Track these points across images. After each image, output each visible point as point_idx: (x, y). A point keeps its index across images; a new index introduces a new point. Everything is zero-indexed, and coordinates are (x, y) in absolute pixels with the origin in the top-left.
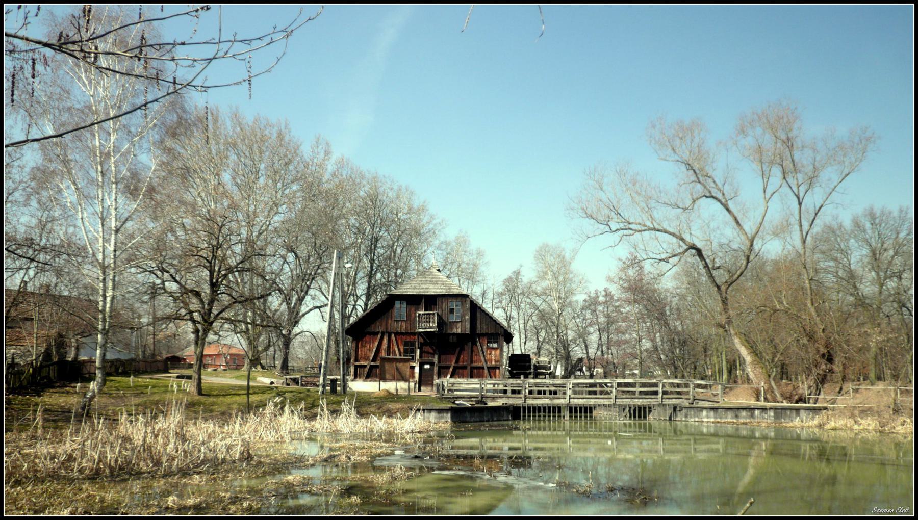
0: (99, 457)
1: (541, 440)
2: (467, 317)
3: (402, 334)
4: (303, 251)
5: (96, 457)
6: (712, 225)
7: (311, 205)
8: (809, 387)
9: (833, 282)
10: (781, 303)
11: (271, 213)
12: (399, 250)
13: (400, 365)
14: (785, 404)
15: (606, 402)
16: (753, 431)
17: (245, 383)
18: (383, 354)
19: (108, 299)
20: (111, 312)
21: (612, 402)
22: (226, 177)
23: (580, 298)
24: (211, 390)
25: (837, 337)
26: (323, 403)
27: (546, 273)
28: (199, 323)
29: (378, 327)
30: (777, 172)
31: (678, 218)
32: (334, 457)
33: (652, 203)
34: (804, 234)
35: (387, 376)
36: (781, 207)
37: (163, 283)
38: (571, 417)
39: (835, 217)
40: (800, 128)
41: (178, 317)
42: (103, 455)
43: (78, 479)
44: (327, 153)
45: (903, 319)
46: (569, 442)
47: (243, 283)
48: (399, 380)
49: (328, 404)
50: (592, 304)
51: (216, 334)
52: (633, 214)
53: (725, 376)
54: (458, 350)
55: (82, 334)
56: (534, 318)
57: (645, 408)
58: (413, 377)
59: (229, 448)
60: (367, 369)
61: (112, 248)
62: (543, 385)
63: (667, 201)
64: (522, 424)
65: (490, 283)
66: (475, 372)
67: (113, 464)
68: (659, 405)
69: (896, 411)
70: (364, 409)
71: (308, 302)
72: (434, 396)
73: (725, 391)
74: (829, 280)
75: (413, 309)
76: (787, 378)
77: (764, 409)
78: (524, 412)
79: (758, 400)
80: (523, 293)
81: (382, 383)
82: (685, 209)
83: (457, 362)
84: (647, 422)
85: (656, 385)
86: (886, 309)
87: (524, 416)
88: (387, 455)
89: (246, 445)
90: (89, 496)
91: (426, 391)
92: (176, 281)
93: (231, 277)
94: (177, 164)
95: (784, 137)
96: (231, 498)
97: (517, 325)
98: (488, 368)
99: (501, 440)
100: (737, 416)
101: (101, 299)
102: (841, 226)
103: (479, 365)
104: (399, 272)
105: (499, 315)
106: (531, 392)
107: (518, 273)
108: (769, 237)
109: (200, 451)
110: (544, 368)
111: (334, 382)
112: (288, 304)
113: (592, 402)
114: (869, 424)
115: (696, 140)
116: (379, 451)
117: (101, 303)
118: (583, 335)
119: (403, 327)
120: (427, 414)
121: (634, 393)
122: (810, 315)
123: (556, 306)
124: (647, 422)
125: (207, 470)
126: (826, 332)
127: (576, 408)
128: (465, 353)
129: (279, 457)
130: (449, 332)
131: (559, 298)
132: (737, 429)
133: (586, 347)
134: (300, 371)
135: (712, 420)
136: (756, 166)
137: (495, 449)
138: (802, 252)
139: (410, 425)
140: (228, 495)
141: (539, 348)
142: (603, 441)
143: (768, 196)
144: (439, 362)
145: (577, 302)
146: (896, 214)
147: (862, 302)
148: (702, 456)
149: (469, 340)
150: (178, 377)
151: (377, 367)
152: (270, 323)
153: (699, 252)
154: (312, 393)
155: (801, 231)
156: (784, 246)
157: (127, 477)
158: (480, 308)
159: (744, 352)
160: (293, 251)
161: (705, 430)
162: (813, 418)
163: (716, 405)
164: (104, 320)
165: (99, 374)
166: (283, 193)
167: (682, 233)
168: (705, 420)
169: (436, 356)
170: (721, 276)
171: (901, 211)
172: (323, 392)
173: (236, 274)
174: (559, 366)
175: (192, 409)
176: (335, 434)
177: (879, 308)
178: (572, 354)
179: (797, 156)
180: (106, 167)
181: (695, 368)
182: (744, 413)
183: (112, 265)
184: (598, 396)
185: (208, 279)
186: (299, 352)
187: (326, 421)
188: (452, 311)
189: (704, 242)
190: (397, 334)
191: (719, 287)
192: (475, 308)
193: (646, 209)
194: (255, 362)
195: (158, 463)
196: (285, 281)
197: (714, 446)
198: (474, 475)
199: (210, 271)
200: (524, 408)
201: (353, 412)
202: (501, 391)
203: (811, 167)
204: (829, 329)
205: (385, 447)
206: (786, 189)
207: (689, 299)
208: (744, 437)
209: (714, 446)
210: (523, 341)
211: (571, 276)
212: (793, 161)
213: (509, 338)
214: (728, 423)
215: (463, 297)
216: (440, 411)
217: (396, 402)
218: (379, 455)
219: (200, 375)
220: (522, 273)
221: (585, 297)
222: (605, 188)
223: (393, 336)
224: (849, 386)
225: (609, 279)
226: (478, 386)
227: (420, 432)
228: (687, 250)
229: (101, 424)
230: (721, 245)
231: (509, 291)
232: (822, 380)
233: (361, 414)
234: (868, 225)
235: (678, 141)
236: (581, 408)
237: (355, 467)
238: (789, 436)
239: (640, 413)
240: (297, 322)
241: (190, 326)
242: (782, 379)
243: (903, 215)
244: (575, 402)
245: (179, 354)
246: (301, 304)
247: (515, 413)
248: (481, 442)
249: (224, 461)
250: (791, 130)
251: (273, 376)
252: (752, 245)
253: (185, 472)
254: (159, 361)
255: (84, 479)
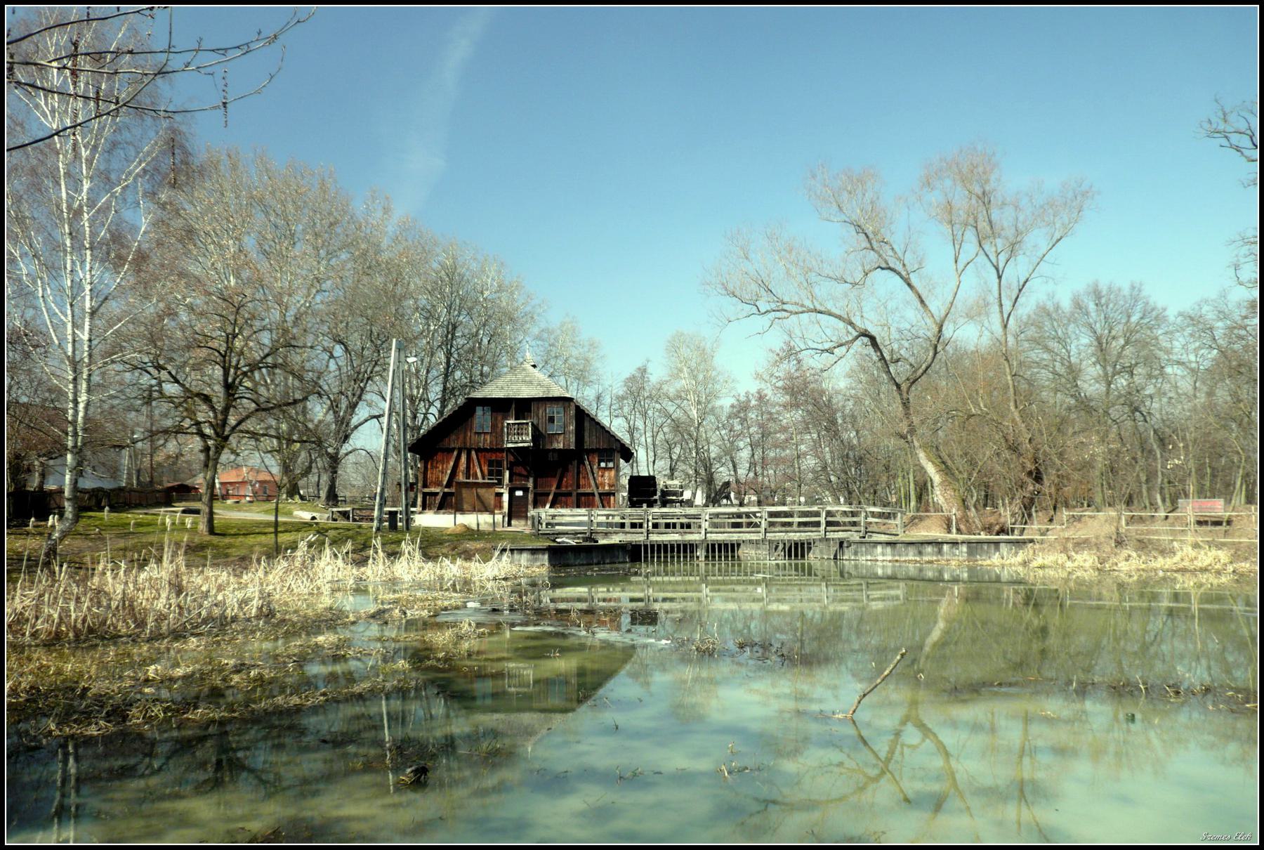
0: (60, 618)
1: (682, 587)
2: (572, 428)
3: (485, 450)
4: (355, 341)
5: (56, 616)
6: (891, 305)
7: (365, 279)
8: (1013, 515)
9: (1048, 380)
10: (976, 404)
11: (301, 288)
12: (485, 341)
13: (482, 491)
14: (983, 536)
15: (754, 537)
16: (941, 572)
17: (273, 519)
18: (461, 478)
19: (81, 406)
20: (85, 423)
21: (760, 536)
22: (250, 242)
23: (725, 403)
24: (228, 526)
25: (1047, 449)
26: (377, 542)
27: (681, 371)
28: (209, 437)
29: (454, 441)
30: (970, 235)
31: (846, 295)
32: (384, 611)
33: (813, 277)
34: (1005, 316)
35: (465, 507)
36: (976, 282)
37: (160, 384)
38: (707, 557)
39: (1051, 296)
40: (999, 180)
41: (179, 430)
42: (65, 611)
43: (30, 646)
44: (386, 210)
45: (1136, 427)
46: (705, 590)
47: (270, 386)
48: (480, 511)
49: (383, 544)
50: (741, 409)
51: (233, 452)
52: (789, 291)
53: (913, 503)
54: (559, 471)
55: (49, 455)
56: (666, 429)
57: (803, 544)
58: (501, 507)
59: (244, 602)
60: (439, 498)
61: (86, 337)
62: (673, 516)
63: (831, 274)
64: (645, 568)
65: (607, 384)
66: (583, 500)
67: (79, 626)
68: (820, 540)
69: (1119, 543)
70: (433, 550)
71: (362, 412)
72: (527, 532)
73: (913, 522)
74: (1044, 376)
75: (500, 418)
76: (993, 506)
77: (955, 544)
78: (646, 552)
79: (949, 532)
80: (650, 397)
81: (458, 516)
82: (854, 284)
83: (559, 487)
84: (806, 562)
85: (817, 514)
86: (1114, 413)
87: (646, 557)
88: (457, 608)
89: (266, 597)
90: (42, 666)
91: (519, 526)
92: (177, 381)
93: (257, 375)
94: (178, 223)
95: (978, 191)
96: (235, 666)
97: (643, 439)
98: (600, 494)
99: (618, 589)
100: (920, 553)
101: (71, 405)
102: (1057, 308)
103: (589, 491)
104: (486, 369)
105: (618, 427)
106: (655, 526)
107: (643, 371)
108: (961, 321)
109: (201, 606)
110: (675, 494)
111: (393, 515)
112: (335, 412)
113: (735, 537)
114: (1085, 562)
115: (869, 195)
116: (446, 603)
117: (71, 412)
118: (730, 452)
119: (485, 441)
120: (516, 556)
121: (790, 524)
122: (1013, 420)
123: (694, 413)
124: (806, 562)
125: (209, 633)
126: (1034, 443)
127: (713, 546)
128: (569, 475)
129: (310, 612)
130: (548, 447)
131: (699, 403)
132: (921, 570)
133: (734, 466)
134: (353, 502)
135: (889, 558)
136: (946, 229)
137: (610, 600)
138: (1003, 340)
139: (491, 572)
140: (232, 662)
141: (672, 470)
142: (751, 588)
143: (961, 267)
144: (535, 486)
145: (722, 407)
146: (1126, 292)
147: (1085, 405)
148: (877, 606)
149: (574, 459)
150: (184, 512)
151: (451, 494)
152: (314, 440)
153: (873, 339)
154: (364, 530)
155: (1001, 312)
156: (981, 331)
157: (98, 641)
158: (588, 415)
159: (931, 469)
160: (341, 342)
161: (880, 572)
162: (1016, 553)
163: (893, 539)
164: (75, 434)
165: (68, 507)
166: (328, 264)
167: (851, 315)
168: (880, 558)
169: (531, 480)
170: (901, 371)
171: (1133, 288)
172: (378, 529)
173: (264, 370)
174: (699, 493)
175: (196, 553)
176: (393, 583)
177: (1106, 413)
178: (716, 476)
179: (995, 216)
180: (76, 226)
181: (875, 492)
182: (929, 549)
183: (86, 360)
184: (744, 529)
185: (221, 378)
186: (351, 476)
187: (381, 567)
188: (551, 420)
189: (880, 328)
190: (478, 450)
191: (898, 386)
192: (582, 417)
193: (805, 284)
194: (293, 491)
195: (141, 624)
196: (330, 383)
197: (892, 592)
198: (566, 632)
199: (224, 368)
200: (646, 546)
201: (418, 555)
202: (616, 525)
203: (1013, 231)
204: (1038, 439)
205: (455, 598)
206: (982, 257)
207: (867, 403)
208: (930, 580)
209: (892, 592)
210: (651, 460)
211: (714, 373)
212: (990, 222)
213: (627, 455)
214: (910, 561)
215: (567, 401)
216: (534, 551)
217: (475, 540)
218: (446, 609)
219: (211, 508)
220: (649, 371)
221: (733, 401)
222: (752, 256)
223: (473, 453)
224: (1065, 514)
225: (758, 376)
226: (586, 519)
227: (505, 579)
228: (857, 338)
229: (63, 574)
230: (900, 331)
231: (632, 393)
232: (1028, 506)
233: (428, 556)
234: (1092, 306)
235: (845, 195)
236: (720, 546)
237: (410, 624)
238: (987, 577)
239: (797, 550)
240: (347, 437)
241: (195, 443)
242: (985, 505)
243: (1135, 293)
244: (713, 537)
245: (189, 482)
246: (353, 412)
247: (634, 553)
248: (590, 592)
249: (234, 619)
250: (987, 181)
251: (315, 509)
252: (940, 331)
253: (178, 635)
254: (159, 491)
255: (37, 646)
